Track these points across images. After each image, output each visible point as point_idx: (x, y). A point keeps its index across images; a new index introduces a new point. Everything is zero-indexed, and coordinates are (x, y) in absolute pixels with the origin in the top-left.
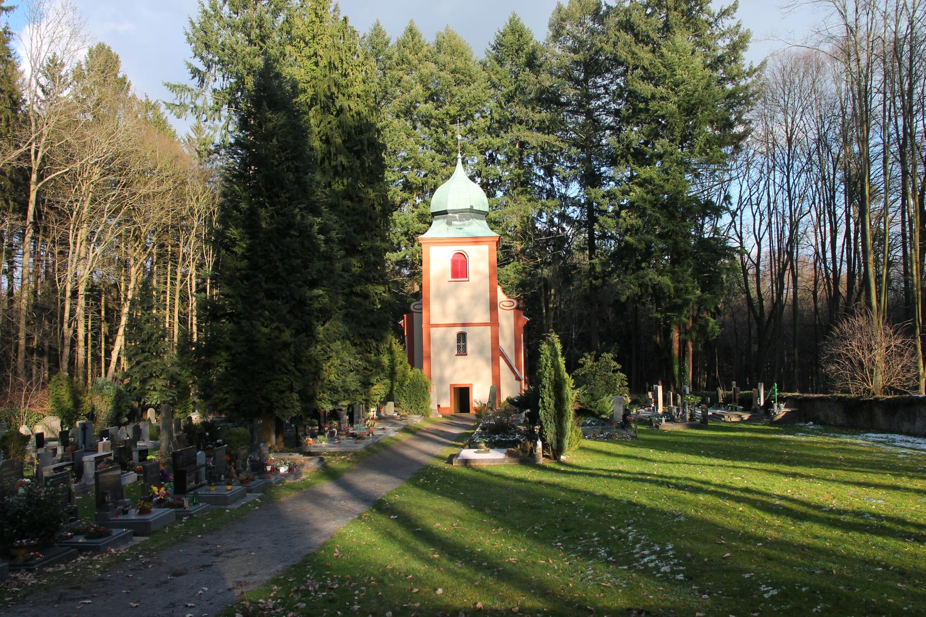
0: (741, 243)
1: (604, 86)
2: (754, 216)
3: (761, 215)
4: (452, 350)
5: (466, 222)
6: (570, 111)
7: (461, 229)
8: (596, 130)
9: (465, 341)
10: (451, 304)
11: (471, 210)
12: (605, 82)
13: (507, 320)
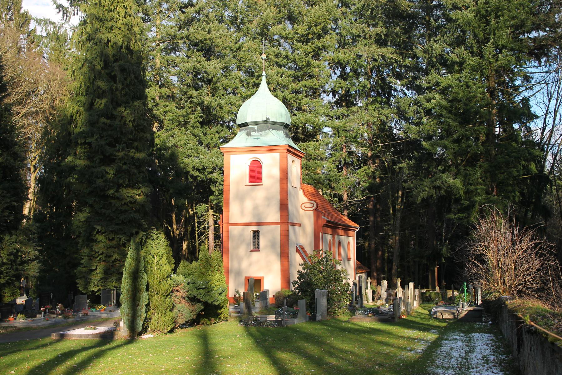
4: (248, 245)
5: (263, 133)
7: (258, 139)
10: (249, 205)
11: (268, 122)
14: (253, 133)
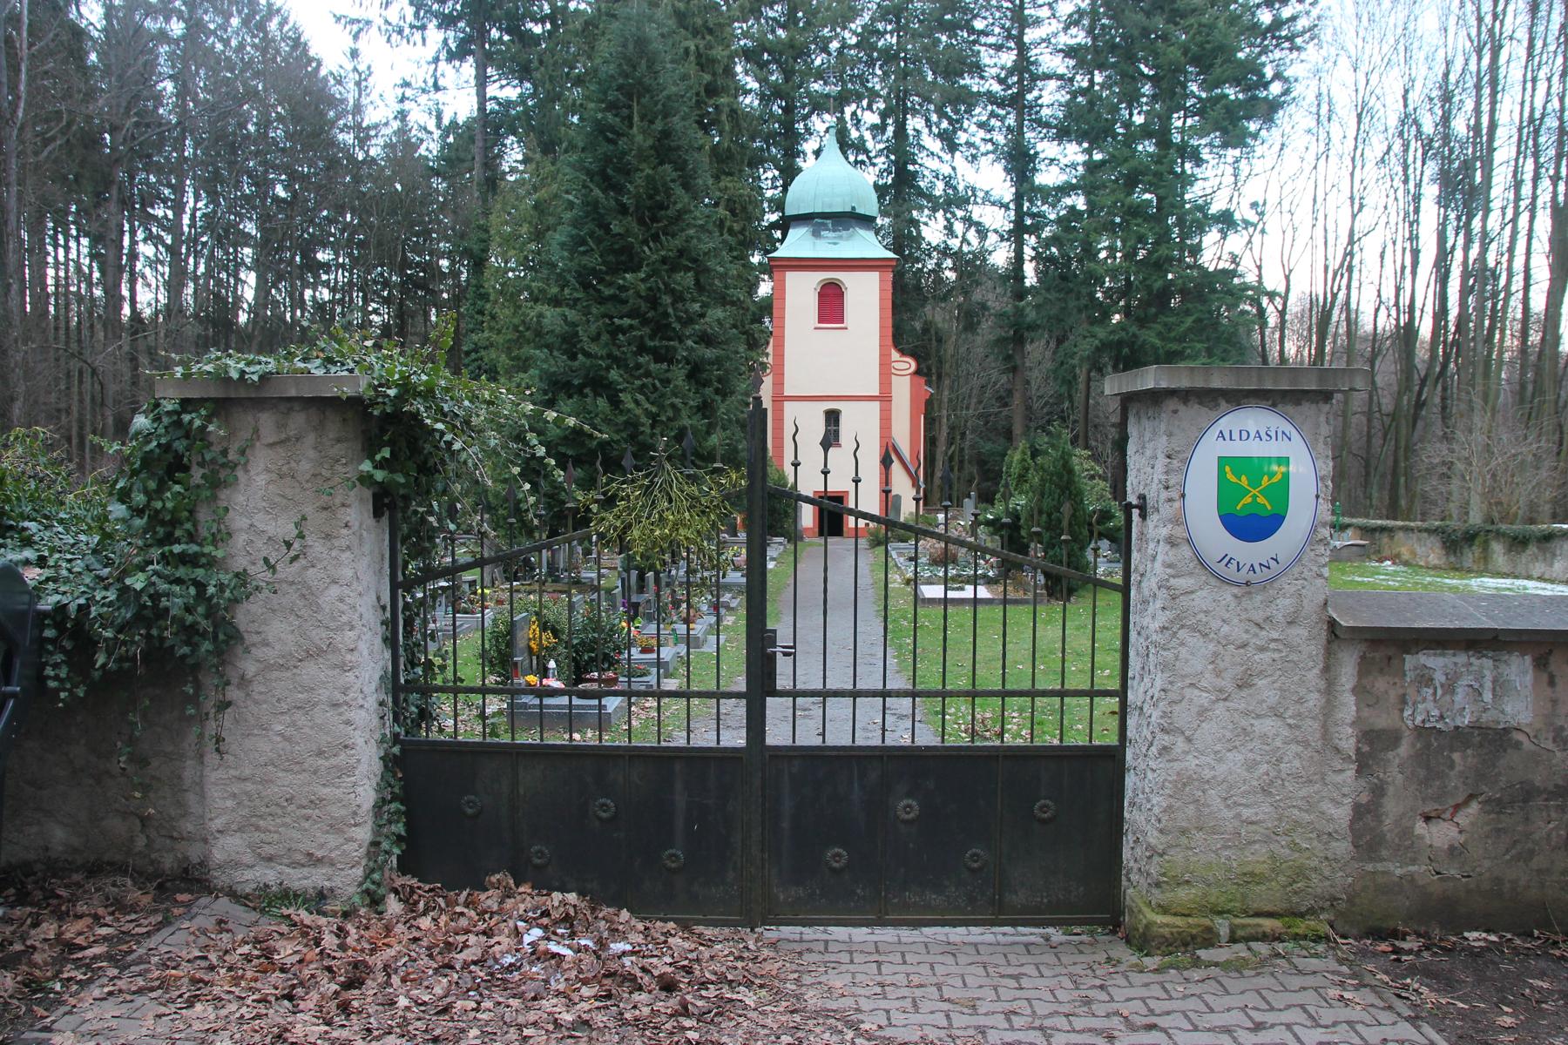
0: (1260, 276)
3: (1295, 229)
5: (844, 233)
6: (990, 46)
8: (1035, 78)
9: (837, 422)
13: (902, 388)
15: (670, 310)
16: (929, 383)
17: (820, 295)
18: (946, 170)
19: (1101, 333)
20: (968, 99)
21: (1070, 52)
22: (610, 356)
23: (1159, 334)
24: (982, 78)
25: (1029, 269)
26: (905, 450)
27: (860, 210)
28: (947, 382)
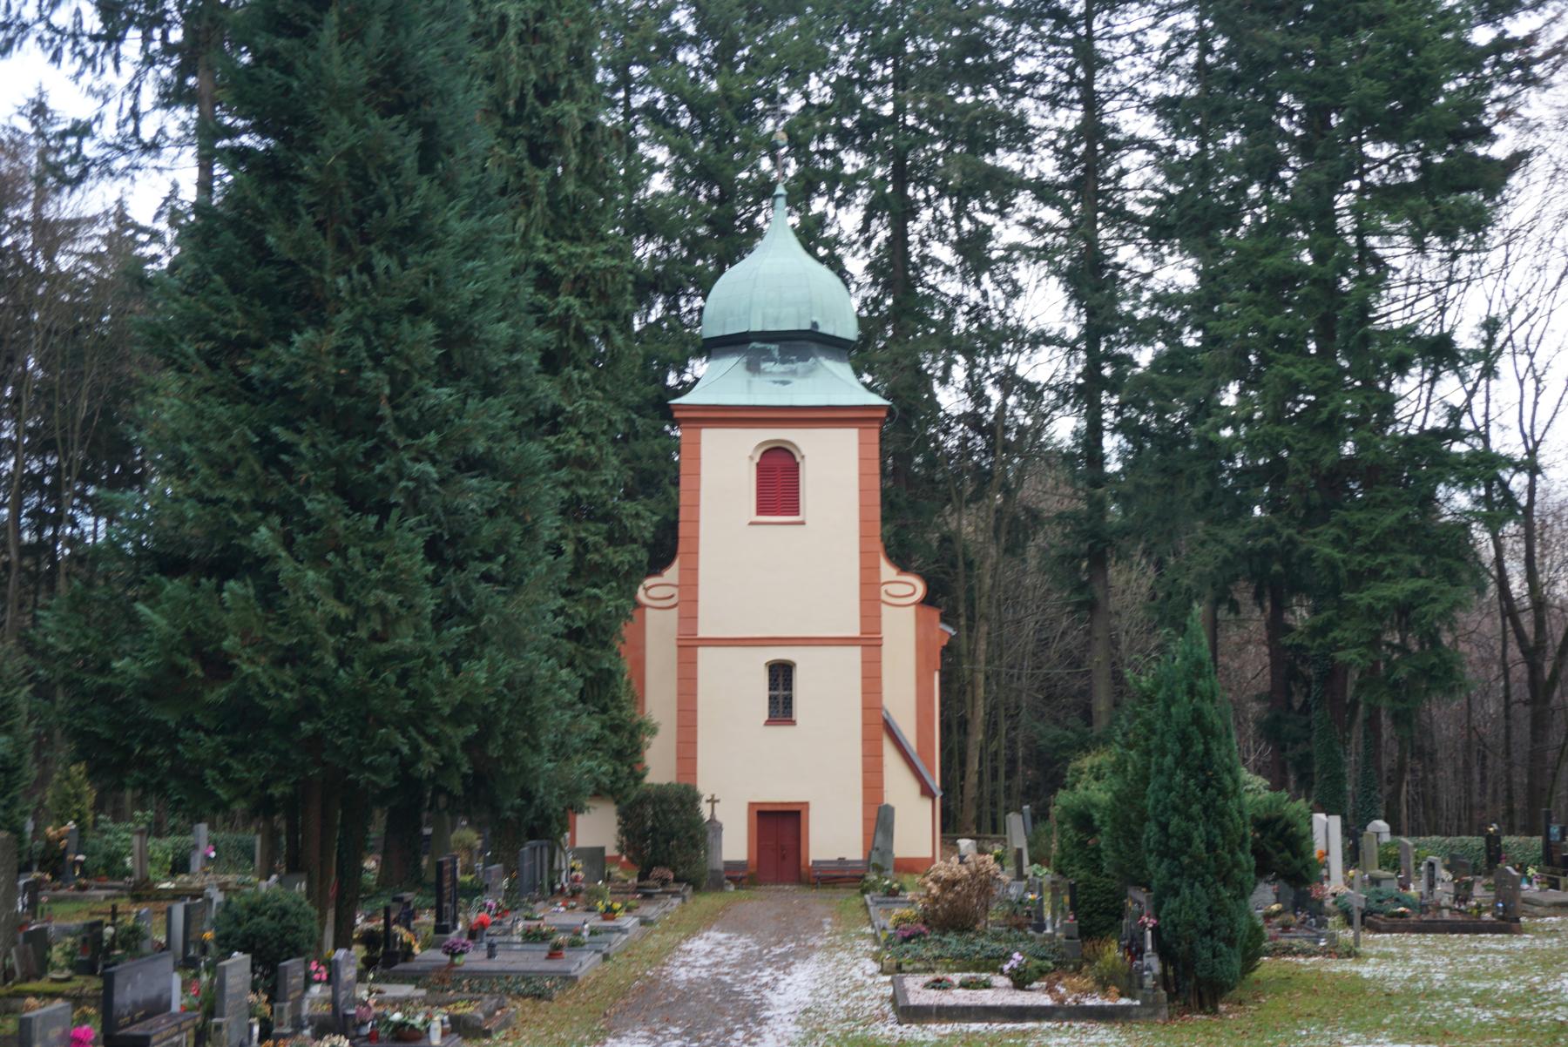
1: (1132, 35)
2: (1521, 382)
5: (800, 366)
7: (784, 383)
8: (1114, 147)
12: (1132, 28)
14: (767, 366)
15: (385, 410)
16: (945, 619)
17: (761, 468)
18: (973, 296)
19: (1232, 536)
20: (1003, 187)
21: (1164, 107)
22: (256, 505)
23: (1336, 542)
24: (1029, 151)
25: (1111, 443)
26: (908, 729)
27: (826, 329)
28: (984, 629)
